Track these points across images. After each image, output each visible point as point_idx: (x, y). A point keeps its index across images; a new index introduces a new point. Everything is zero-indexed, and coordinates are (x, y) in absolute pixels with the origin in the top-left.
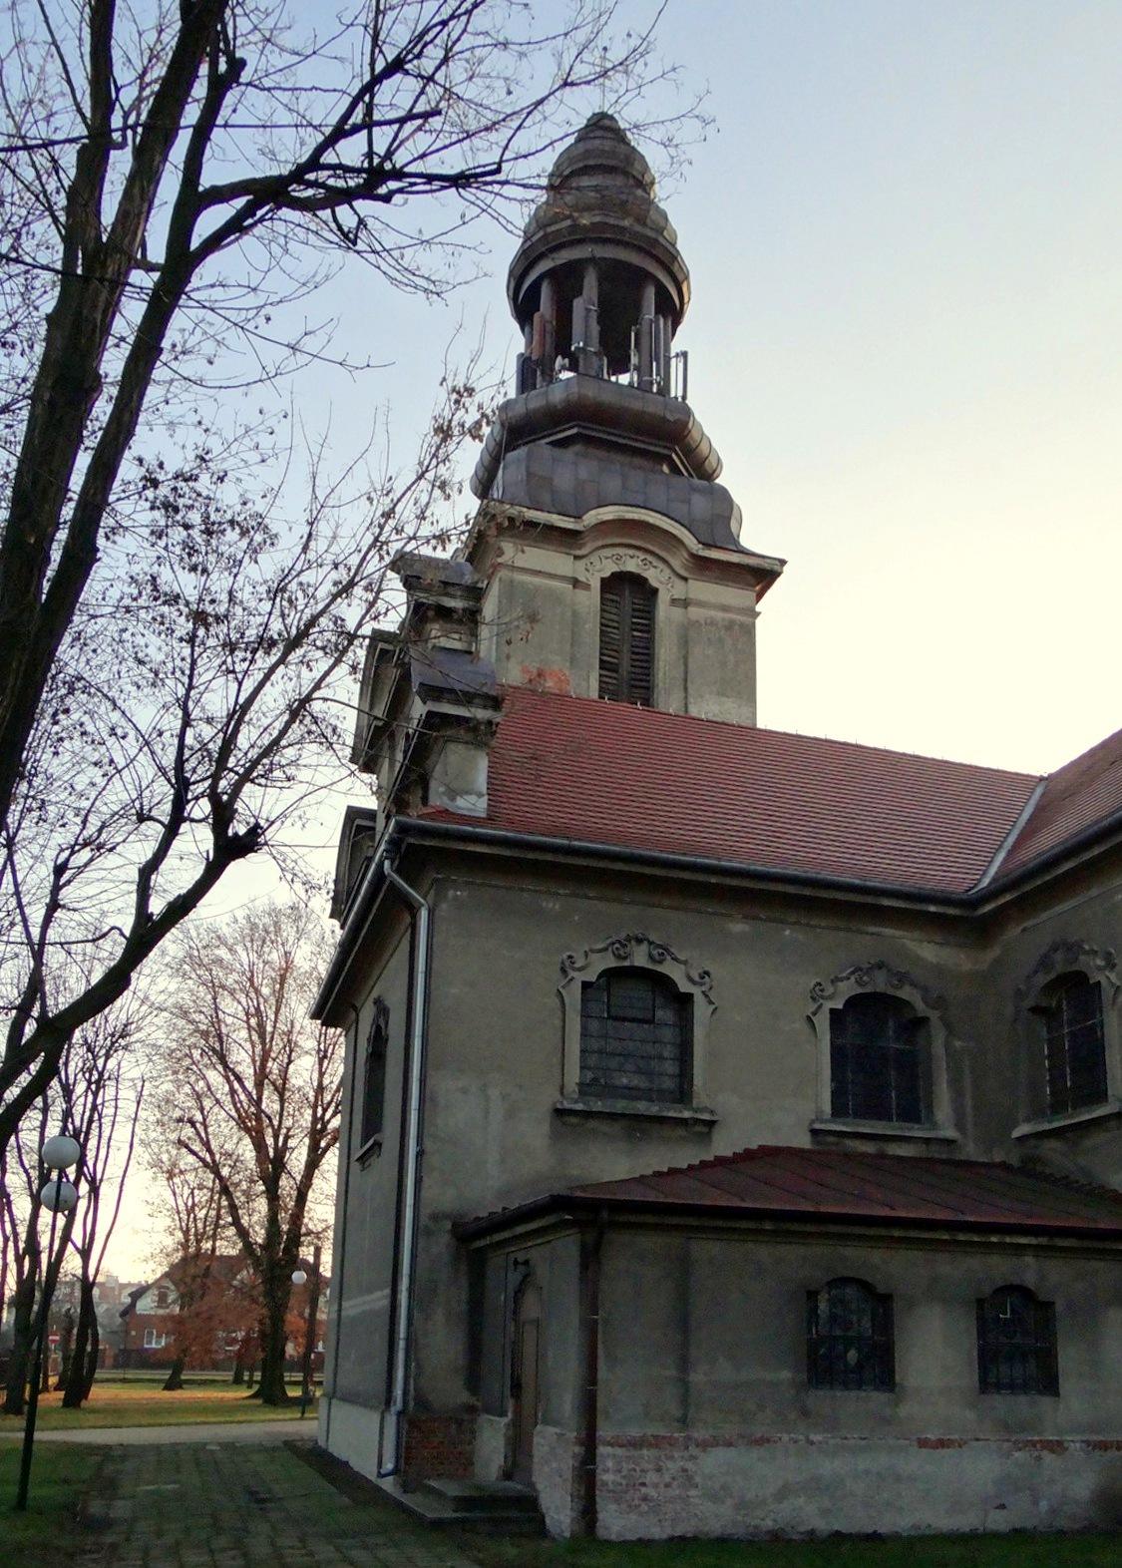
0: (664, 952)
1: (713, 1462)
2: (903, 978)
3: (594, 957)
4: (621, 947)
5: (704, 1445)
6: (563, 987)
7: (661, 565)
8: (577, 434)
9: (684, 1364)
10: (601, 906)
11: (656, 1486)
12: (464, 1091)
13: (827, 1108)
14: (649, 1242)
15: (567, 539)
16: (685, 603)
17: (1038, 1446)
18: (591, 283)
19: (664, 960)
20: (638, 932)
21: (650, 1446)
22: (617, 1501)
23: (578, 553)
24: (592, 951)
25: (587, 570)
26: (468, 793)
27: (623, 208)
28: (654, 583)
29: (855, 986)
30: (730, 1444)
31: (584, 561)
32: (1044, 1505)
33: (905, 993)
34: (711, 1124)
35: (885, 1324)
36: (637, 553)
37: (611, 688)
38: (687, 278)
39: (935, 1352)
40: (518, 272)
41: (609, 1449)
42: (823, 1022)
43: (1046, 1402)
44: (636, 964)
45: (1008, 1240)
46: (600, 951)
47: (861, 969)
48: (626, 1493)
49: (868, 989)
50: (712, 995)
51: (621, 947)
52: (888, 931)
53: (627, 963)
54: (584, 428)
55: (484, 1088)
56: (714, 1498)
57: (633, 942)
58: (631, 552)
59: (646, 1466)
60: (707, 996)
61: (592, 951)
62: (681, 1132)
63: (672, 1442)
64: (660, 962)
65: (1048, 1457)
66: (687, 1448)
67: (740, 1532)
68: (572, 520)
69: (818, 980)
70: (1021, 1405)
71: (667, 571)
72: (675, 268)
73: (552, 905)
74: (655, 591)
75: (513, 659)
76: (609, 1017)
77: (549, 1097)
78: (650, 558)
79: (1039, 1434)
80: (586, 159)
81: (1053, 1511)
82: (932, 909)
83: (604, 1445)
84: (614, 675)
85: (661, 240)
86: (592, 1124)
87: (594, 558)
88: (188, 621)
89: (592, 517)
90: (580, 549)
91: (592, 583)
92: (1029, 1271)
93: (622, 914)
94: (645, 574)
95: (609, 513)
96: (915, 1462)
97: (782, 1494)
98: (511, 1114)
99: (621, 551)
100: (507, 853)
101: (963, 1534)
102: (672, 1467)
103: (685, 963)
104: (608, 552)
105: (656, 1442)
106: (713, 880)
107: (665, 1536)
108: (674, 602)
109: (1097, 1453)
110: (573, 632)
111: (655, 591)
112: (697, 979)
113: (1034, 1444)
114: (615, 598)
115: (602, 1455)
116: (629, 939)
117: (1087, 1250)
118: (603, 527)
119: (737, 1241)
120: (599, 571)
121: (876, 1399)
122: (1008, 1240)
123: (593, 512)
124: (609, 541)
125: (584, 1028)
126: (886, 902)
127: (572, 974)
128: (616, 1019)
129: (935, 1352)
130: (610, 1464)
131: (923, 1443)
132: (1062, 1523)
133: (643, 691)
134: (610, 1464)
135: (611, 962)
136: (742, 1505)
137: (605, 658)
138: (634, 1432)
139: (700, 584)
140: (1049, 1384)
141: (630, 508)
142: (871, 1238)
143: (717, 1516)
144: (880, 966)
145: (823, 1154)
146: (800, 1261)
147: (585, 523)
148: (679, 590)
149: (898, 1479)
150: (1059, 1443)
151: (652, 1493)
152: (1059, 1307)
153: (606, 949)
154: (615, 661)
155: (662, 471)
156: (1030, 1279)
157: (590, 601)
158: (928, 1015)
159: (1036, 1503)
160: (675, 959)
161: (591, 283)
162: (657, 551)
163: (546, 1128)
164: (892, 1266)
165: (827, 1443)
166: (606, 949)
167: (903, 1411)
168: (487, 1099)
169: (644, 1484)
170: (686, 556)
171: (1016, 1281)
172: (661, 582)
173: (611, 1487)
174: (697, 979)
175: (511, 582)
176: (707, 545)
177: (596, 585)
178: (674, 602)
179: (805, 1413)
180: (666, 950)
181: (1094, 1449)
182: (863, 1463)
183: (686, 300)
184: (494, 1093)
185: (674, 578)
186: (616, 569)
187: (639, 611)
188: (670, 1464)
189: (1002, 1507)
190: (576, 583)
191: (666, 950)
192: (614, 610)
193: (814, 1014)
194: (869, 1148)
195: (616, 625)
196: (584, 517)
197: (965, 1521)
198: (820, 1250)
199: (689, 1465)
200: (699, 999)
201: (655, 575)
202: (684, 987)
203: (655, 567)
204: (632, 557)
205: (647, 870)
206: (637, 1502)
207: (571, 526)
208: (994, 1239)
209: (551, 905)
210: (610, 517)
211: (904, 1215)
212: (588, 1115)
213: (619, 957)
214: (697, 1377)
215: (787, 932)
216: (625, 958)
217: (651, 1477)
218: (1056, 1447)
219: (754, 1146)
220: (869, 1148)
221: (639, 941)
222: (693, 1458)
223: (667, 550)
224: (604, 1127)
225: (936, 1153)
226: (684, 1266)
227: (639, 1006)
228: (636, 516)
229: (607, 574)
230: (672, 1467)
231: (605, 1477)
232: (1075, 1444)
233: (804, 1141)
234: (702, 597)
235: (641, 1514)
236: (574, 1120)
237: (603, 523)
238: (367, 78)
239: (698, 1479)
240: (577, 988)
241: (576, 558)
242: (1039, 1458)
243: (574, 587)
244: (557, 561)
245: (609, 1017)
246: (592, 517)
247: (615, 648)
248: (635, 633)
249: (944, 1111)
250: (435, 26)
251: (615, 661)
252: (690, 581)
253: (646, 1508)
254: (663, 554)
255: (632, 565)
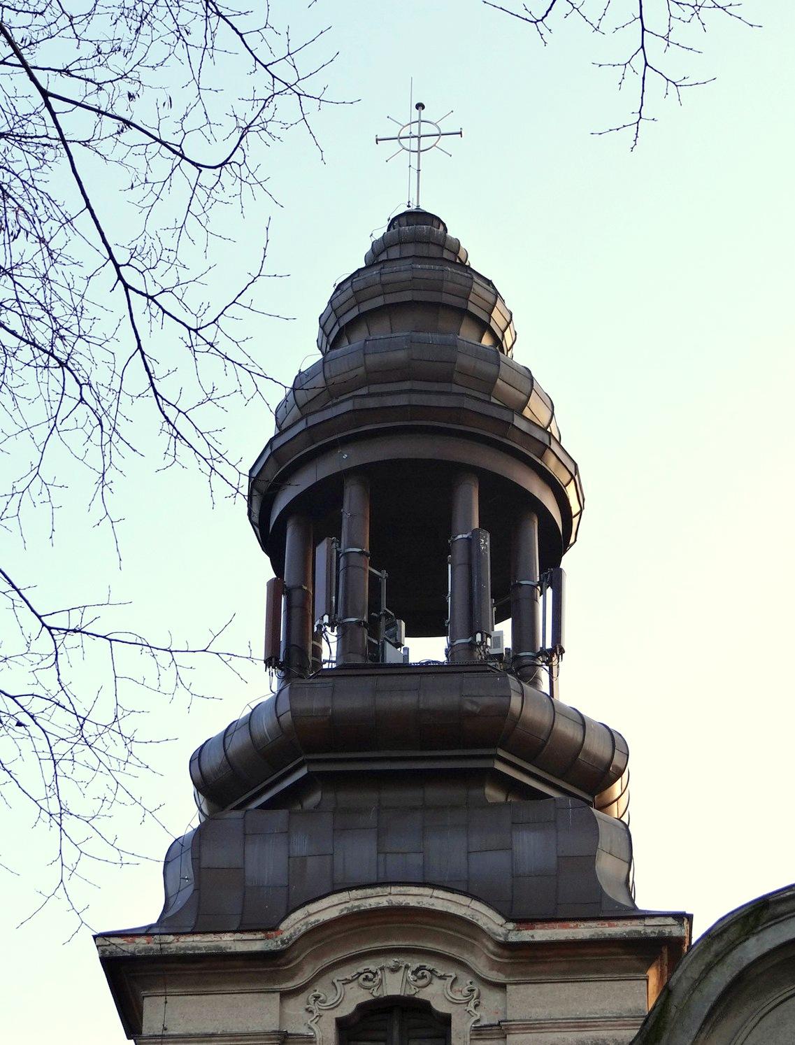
18: (354, 503)
23: (290, 985)
25: (310, 1011)
28: (440, 1006)
31: (302, 998)
36: (403, 960)
38: (574, 476)
40: (272, 474)
58: (391, 962)
71: (466, 981)
72: (551, 464)
74: (446, 1020)
80: (358, 303)
85: (518, 422)
87: (319, 989)
88: (488, 928)
89: (295, 924)
90: (292, 978)
94: (424, 995)
95: (328, 909)
104: (348, 972)
111: (446, 1020)
118: (319, 933)
123: (299, 914)
139: (531, 990)
141: (369, 891)
147: (286, 935)
161: (354, 503)
170: (491, 946)
172: (454, 1002)
176: (525, 921)
183: (575, 508)
186: (363, 996)
196: (283, 926)
201: (437, 995)
203: (442, 978)
204: (394, 970)
207: (257, 947)
210: (334, 913)
228: (383, 902)
229: (347, 1009)
238: (23, 70)
241: (286, 995)
246: (295, 924)
250: (216, 8)
252: (509, 987)
254: (453, 951)
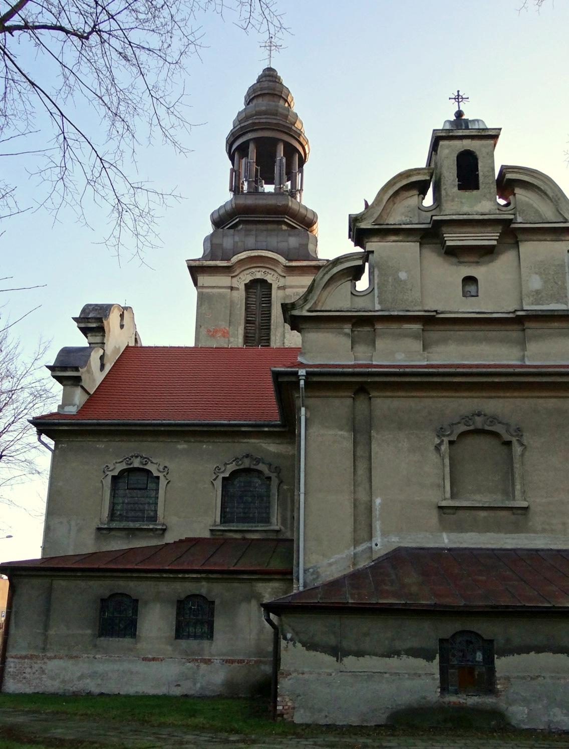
0: (146, 460)
1: (53, 665)
2: (258, 461)
3: (118, 465)
4: (128, 460)
5: (50, 658)
6: (103, 479)
7: (273, 273)
8: (239, 220)
9: (46, 627)
10: (121, 444)
11: (30, 673)
12: (61, 523)
13: (218, 520)
14: (36, 582)
15: (227, 270)
16: (283, 288)
17: (199, 661)
19: (148, 463)
20: (136, 453)
21: (28, 658)
22: (14, 679)
24: (116, 463)
26: (70, 405)
27: (275, 114)
28: (269, 281)
29: (235, 466)
30: (61, 658)
32: (198, 685)
33: (261, 467)
34: (164, 530)
35: (212, 614)
36: (261, 269)
37: (251, 331)
39: (155, 623)
41: (12, 660)
42: (219, 484)
43: (206, 643)
44: (135, 466)
45: (187, 576)
46: (119, 463)
47: (238, 459)
48: (17, 676)
49: (241, 467)
50: (168, 477)
51: (128, 460)
52: (253, 441)
53: (131, 466)
54: (240, 217)
55: (69, 522)
56: (53, 678)
57: (134, 457)
58: (258, 269)
59: (26, 666)
60: (165, 477)
61: (116, 463)
62: (151, 534)
63: (37, 657)
64: (146, 464)
65: (203, 666)
66: (43, 659)
67: (61, 691)
68: (226, 262)
69: (218, 465)
70: (193, 644)
71: (276, 275)
73: (101, 446)
74: (271, 284)
75: (203, 327)
76: (128, 489)
77: (96, 523)
78: (267, 270)
79: (201, 656)
81: (202, 688)
82: (266, 429)
83: (10, 658)
84: (253, 325)
86: (113, 533)
87: (240, 276)
89: (235, 259)
91: (240, 288)
92: (203, 588)
93: (131, 446)
96: (140, 667)
97: (80, 678)
98: (79, 530)
99: (253, 270)
100: (76, 428)
101: (149, 695)
102: (36, 667)
103: (156, 464)
104: (248, 272)
105: (31, 657)
106: (163, 429)
107: (31, 692)
108: (279, 288)
109: (228, 664)
110: (230, 310)
112: (162, 470)
113: (197, 660)
114: (253, 291)
115: (9, 662)
116: (132, 457)
117: (86, 576)
119: (136, 581)
120: (244, 281)
121: (127, 641)
122: (187, 576)
124: (252, 266)
125: (157, 493)
126: (243, 429)
127: (108, 473)
128: (130, 489)
129: (155, 623)
130: (12, 665)
131: (145, 659)
132: (208, 693)
133: (266, 330)
134: (12, 665)
135: (124, 466)
136: (64, 681)
137: (248, 319)
138: (24, 653)
140: (210, 636)
142: (141, 577)
143: (52, 685)
144: (247, 456)
145: (216, 542)
146: (101, 587)
147: (232, 262)
148: (282, 282)
149: (132, 673)
150: (209, 660)
151: (28, 676)
152: (217, 602)
153: (122, 461)
154: (254, 319)
155: (282, 230)
156: (204, 592)
157: (240, 295)
158: (270, 475)
159: (195, 684)
160: (152, 463)
162: (268, 266)
163: (93, 536)
164: (133, 587)
165: (102, 658)
166: (122, 461)
167: (139, 646)
168: (70, 525)
169: (25, 673)
170: (282, 266)
171: (197, 592)
173: (12, 674)
174: (162, 470)
175: (202, 293)
177: (242, 287)
178: (279, 288)
179: (95, 646)
180: (148, 459)
181: (226, 662)
182: (116, 667)
184: (73, 523)
185: (279, 277)
187: (265, 294)
188: (36, 665)
189: (179, 685)
190: (232, 288)
191: (148, 459)
192: (254, 296)
193: (215, 480)
194: (238, 536)
195: (254, 303)
196: (232, 260)
197: (161, 691)
198: (108, 582)
199: (44, 667)
200: (162, 479)
201: (269, 278)
202: (155, 474)
203: (270, 274)
204: (259, 272)
205: (134, 428)
206: (21, 679)
207: (225, 265)
208: (180, 576)
209: (100, 446)
210: (244, 257)
211: (213, 568)
212: (110, 529)
213: (127, 464)
214: (51, 632)
215: (204, 446)
216: (130, 464)
217: (28, 670)
218: (208, 662)
219: (183, 538)
220: (238, 536)
221: (137, 457)
222: (45, 663)
223: (274, 265)
224: (119, 534)
225: (272, 536)
226: (50, 590)
227: (134, 484)
228: (256, 254)
229: (247, 281)
230: (36, 667)
231: (9, 670)
232: (217, 662)
233: (207, 535)
234: (293, 284)
235: (24, 684)
236: (105, 532)
237: (242, 260)
239: (46, 671)
240: (109, 479)
242: (198, 666)
243: (231, 290)
244: (223, 280)
245: (128, 489)
246: (235, 259)
247: (254, 313)
248: (263, 305)
249: (274, 520)
251: (254, 319)
253: (25, 682)
255: (259, 276)
